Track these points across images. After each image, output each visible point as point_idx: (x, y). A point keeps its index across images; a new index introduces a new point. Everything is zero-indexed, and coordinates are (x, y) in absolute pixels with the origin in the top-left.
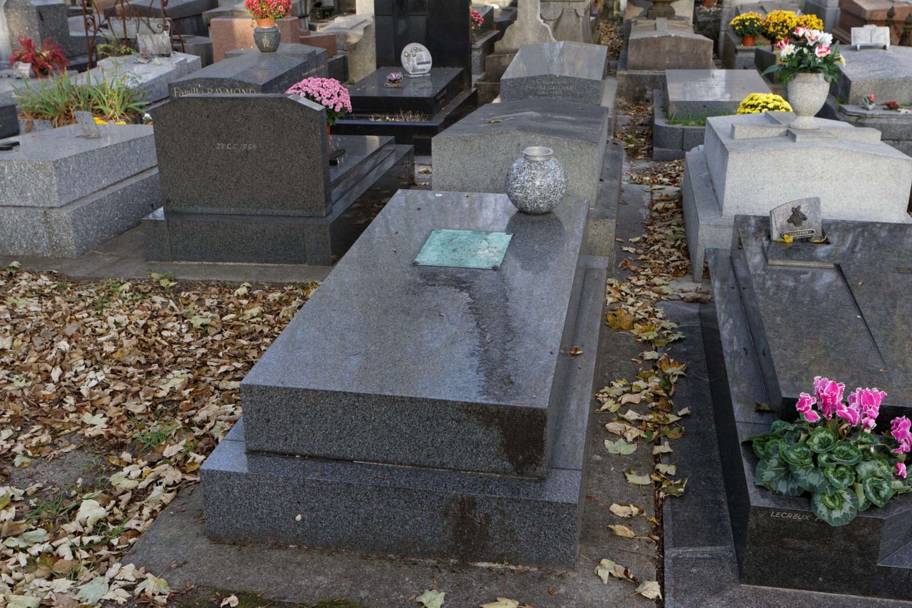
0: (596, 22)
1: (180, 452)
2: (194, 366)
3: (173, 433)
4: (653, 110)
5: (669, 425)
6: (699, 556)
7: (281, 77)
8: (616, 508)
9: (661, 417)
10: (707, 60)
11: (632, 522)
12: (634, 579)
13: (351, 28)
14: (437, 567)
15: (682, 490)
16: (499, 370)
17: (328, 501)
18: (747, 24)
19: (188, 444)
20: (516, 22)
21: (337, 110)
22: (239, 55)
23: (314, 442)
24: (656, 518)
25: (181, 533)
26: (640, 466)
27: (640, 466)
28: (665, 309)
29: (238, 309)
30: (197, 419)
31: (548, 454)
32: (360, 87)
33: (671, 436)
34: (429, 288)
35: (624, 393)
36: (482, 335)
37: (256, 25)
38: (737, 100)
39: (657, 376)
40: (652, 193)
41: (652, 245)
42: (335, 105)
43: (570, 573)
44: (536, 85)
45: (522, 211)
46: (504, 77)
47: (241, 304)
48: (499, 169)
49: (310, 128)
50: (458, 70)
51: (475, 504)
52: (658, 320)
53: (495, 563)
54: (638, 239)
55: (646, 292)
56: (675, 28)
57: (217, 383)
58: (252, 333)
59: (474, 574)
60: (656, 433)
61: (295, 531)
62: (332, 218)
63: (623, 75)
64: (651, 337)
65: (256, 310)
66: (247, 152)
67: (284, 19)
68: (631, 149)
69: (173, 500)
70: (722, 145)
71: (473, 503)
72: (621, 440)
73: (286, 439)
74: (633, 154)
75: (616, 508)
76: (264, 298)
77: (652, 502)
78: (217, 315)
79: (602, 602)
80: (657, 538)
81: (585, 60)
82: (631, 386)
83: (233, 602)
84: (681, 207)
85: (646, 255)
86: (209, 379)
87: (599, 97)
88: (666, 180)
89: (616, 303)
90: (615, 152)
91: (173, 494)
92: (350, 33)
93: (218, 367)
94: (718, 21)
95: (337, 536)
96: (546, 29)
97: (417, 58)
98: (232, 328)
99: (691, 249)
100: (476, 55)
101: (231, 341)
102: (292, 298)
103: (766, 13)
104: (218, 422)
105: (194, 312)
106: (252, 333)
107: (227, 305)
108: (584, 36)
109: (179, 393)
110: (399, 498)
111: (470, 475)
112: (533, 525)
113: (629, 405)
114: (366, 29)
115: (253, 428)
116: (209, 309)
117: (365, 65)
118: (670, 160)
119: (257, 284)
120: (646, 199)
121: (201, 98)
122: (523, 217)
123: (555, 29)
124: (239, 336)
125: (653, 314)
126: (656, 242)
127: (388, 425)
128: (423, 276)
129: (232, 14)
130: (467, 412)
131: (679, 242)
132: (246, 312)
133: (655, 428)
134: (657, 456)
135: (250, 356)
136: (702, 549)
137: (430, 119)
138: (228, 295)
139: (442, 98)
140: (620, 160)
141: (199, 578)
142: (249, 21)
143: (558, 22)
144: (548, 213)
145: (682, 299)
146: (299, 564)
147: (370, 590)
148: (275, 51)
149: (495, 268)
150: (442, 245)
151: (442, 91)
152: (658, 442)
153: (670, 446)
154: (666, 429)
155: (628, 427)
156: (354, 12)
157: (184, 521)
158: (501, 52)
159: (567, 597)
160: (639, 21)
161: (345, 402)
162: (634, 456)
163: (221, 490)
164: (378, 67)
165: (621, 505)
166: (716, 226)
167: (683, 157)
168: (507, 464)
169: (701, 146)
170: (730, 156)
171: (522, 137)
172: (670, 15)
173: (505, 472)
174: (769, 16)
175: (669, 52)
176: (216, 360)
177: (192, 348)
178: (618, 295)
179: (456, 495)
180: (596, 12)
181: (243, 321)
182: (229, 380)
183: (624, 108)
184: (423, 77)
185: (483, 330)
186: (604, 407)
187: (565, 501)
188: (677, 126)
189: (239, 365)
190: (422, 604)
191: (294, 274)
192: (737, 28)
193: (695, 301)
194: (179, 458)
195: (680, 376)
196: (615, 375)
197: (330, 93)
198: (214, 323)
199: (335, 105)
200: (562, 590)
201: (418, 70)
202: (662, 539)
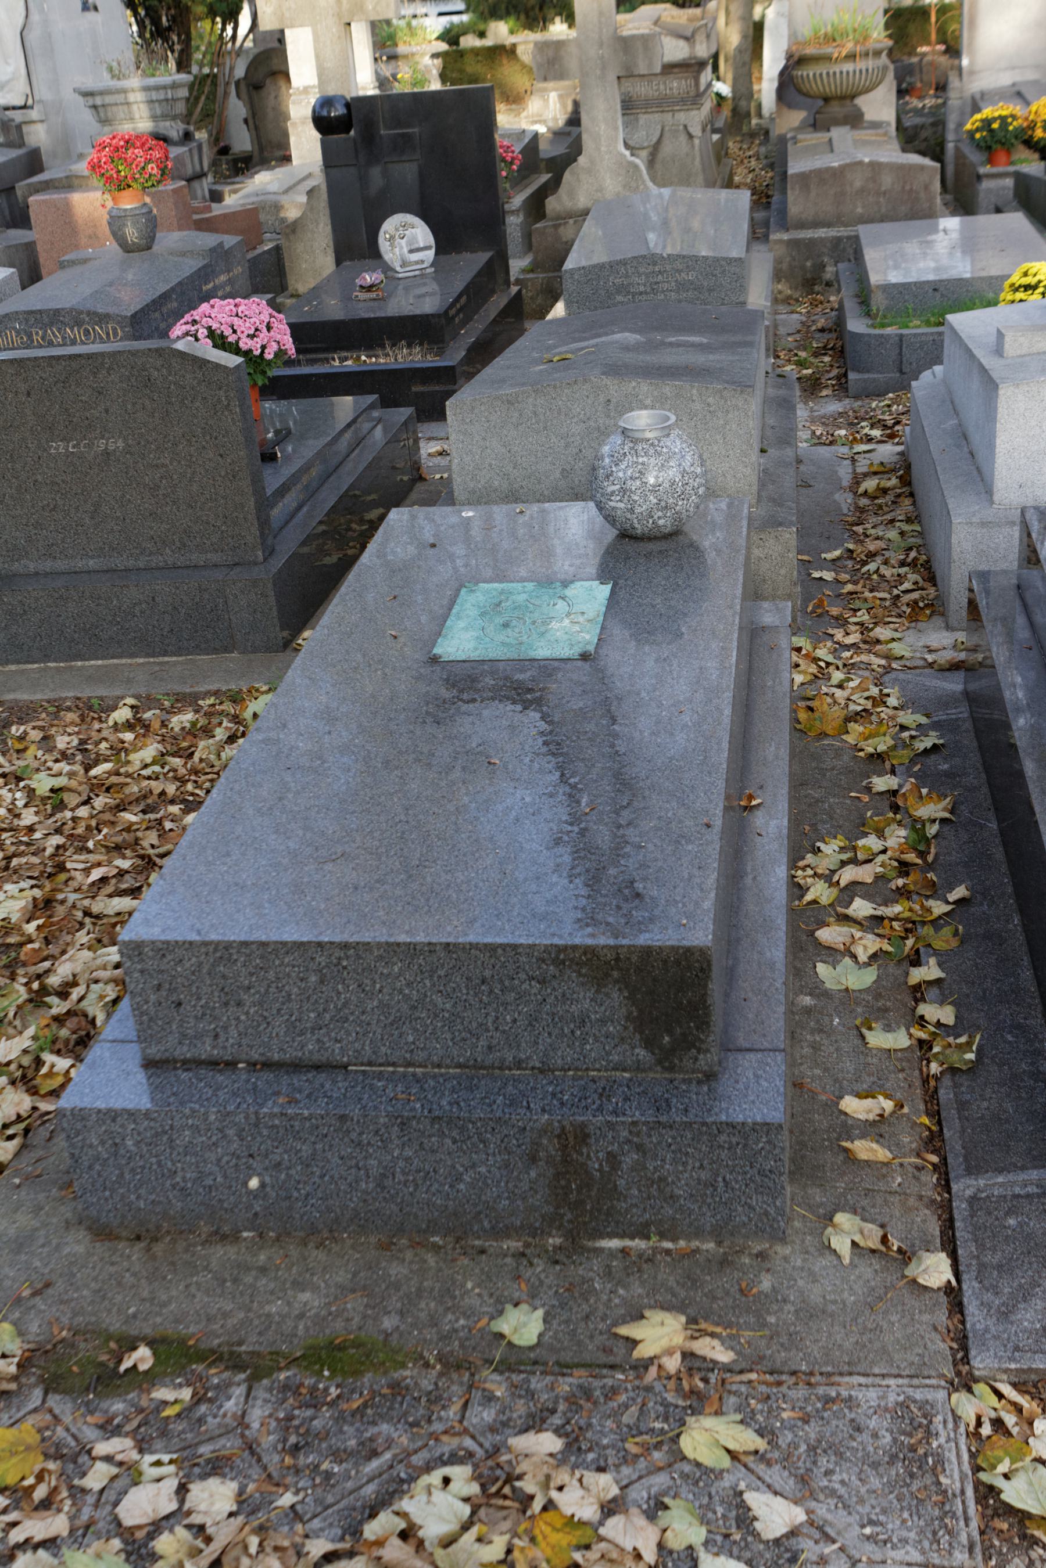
0: (722, 142)
1: (25, 1052)
2: (42, 872)
3: (11, 1014)
4: (841, 303)
5: (931, 921)
6: (1017, 1190)
7: (165, 297)
8: (851, 1105)
9: (917, 907)
10: (931, 200)
11: (884, 1129)
12: (900, 1250)
13: (286, 192)
14: (523, 1255)
15: (971, 1056)
16: (612, 871)
17: (306, 1150)
18: (995, 126)
19: (41, 1034)
20: (581, 159)
21: (269, 355)
22: (85, 261)
23: (270, 1037)
24: (928, 1114)
25: (35, 1223)
26: (887, 1010)
27: (887, 1010)
28: (902, 689)
29: (119, 750)
30: (54, 981)
31: (717, 1018)
32: (309, 303)
33: (938, 944)
34: (464, 707)
35: (843, 864)
36: (573, 798)
37: (110, 204)
38: (994, 270)
39: (900, 823)
40: (853, 460)
41: (864, 563)
42: (263, 347)
43: (778, 1248)
44: (627, 276)
45: (626, 535)
46: (569, 264)
47: (123, 742)
48: (575, 451)
49: (219, 401)
50: (482, 257)
51: (587, 1136)
52: (891, 712)
53: (632, 1238)
54: (837, 553)
55: (864, 658)
56: (865, 143)
57: (86, 902)
58: (145, 797)
59: (596, 1264)
60: (910, 942)
61: (249, 1207)
62: (278, 562)
63: (781, 241)
64: (882, 748)
65: (150, 751)
66: (107, 453)
67: (161, 188)
68: (809, 378)
69: (17, 1155)
70: (983, 370)
71: (583, 1136)
72: (847, 960)
73: (216, 1036)
74: (812, 387)
75: (851, 1105)
76: (164, 724)
77: (918, 1083)
78: (78, 768)
79: (844, 1302)
80: (934, 1159)
81: (711, 221)
82: (854, 849)
83: (142, 1359)
84: (910, 484)
85: (855, 583)
86: (72, 897)
87: (743, 289)
88: (876, 433)
89: (810, 683)
90: (782, 392)
91: (16, 1142)
92: (284, 200)
93: (87, 871)
94: (939, 124)
95: (329, 1210)
96: (636, 166)
97: (407, 240)
98: (108, 790)
99: (936, 566)
100: (514, 223)
101: (108, 816)
102: (215, 721)
103: (1028, 103)
104: (93, 986)
105: (36, 764)
106: (145, 797)
107: (97, 744)
108: (704, 170)
109: (19, 929)
110: (442, 1134)
111: (574, 1079)
112: (702, 1167)
113: (853, 889)
114: (310, 193)
115: (151, 1020)
116: (64, 756)
117: (315, 261)
118: (880, 394)
119: (148, 697)
120: (845, 473)
121: (12, 361)
122: (629, 546)
123: (651, 163)
124: (121, 807)
125: (880, 701)
126: (872, 555)
127: (407, 998)
128: (451, 683)
129: (69, 184)
130: (557, 962)
131: (913, 554)
132: (132, 757)
133: (907, 930)
134: (917, 988)
135: (145, 844)
136: (1022, 1176)
137: (440, 353)
138: (96, 725)
139: (459, 311)
140: (793, 408)
141: (75, 1314)
142: (98, 194)
143: (655, 149)
144: (674, 534)
145: (931, 665)
146: (263, 1270)
147: (401, 1313)
148: (149, 248)
149: (585, 657)
150: (483, 614)
151: (457, 300)
152: (916, 961)
153: (940, 965)
154: (927, 931)
155: (858, 934)
156: (287, 159)
157: (41, 1196)
158: (558, 217)
159: (776, 1297)
160: (800, 137)
161: (322, 960)
162: (875, 991)
163: (103, 1143)
164: (338, 262)
165: (859, 1096)
166: (983, 524)
167: (907, 388)
168: (641, 1053)
169: (938, 369)
170: (1001, 392)
171: (613, 388)
172: (855, 120)
173: (639, 1067)
174: (1034, 108)
175: (862, 191)
176: (82, 857)
177: (37, 835)
178: (813, 669)
179: (550, 1123)
180: (720, 124)
181: (128, 775)
182: (110, 896)
183: (787, 300)
184: (422, 276)
185: (574, 787)
186: (809, 897)
187: (759, 1119)
188: (889, 330)
189: (125, 864)
190: (501, 1336)
191: (214, 673)
192: (978, 136)
193: (955, 667)
194: (26, 1061)
195: (943, 821)
196: (823, 828)
197: (258, 325)
198: (73, 784)
199: (263, 347)
200: (766, 1284)
201: (411, 264)
202: (944, 1160)
